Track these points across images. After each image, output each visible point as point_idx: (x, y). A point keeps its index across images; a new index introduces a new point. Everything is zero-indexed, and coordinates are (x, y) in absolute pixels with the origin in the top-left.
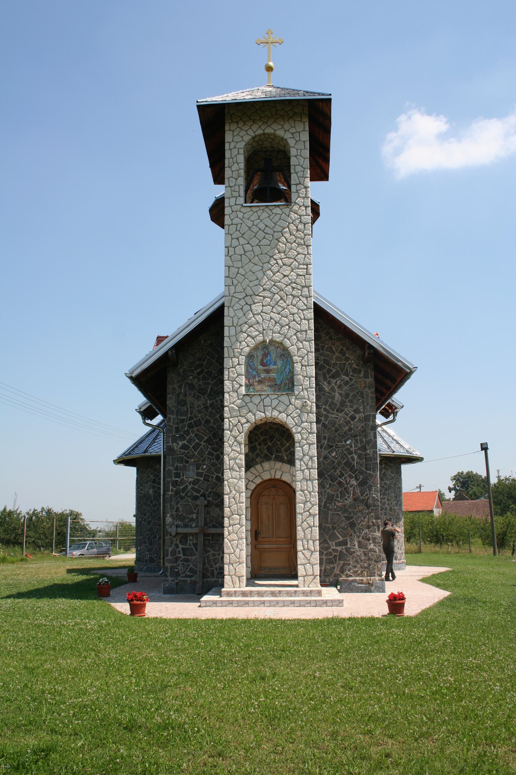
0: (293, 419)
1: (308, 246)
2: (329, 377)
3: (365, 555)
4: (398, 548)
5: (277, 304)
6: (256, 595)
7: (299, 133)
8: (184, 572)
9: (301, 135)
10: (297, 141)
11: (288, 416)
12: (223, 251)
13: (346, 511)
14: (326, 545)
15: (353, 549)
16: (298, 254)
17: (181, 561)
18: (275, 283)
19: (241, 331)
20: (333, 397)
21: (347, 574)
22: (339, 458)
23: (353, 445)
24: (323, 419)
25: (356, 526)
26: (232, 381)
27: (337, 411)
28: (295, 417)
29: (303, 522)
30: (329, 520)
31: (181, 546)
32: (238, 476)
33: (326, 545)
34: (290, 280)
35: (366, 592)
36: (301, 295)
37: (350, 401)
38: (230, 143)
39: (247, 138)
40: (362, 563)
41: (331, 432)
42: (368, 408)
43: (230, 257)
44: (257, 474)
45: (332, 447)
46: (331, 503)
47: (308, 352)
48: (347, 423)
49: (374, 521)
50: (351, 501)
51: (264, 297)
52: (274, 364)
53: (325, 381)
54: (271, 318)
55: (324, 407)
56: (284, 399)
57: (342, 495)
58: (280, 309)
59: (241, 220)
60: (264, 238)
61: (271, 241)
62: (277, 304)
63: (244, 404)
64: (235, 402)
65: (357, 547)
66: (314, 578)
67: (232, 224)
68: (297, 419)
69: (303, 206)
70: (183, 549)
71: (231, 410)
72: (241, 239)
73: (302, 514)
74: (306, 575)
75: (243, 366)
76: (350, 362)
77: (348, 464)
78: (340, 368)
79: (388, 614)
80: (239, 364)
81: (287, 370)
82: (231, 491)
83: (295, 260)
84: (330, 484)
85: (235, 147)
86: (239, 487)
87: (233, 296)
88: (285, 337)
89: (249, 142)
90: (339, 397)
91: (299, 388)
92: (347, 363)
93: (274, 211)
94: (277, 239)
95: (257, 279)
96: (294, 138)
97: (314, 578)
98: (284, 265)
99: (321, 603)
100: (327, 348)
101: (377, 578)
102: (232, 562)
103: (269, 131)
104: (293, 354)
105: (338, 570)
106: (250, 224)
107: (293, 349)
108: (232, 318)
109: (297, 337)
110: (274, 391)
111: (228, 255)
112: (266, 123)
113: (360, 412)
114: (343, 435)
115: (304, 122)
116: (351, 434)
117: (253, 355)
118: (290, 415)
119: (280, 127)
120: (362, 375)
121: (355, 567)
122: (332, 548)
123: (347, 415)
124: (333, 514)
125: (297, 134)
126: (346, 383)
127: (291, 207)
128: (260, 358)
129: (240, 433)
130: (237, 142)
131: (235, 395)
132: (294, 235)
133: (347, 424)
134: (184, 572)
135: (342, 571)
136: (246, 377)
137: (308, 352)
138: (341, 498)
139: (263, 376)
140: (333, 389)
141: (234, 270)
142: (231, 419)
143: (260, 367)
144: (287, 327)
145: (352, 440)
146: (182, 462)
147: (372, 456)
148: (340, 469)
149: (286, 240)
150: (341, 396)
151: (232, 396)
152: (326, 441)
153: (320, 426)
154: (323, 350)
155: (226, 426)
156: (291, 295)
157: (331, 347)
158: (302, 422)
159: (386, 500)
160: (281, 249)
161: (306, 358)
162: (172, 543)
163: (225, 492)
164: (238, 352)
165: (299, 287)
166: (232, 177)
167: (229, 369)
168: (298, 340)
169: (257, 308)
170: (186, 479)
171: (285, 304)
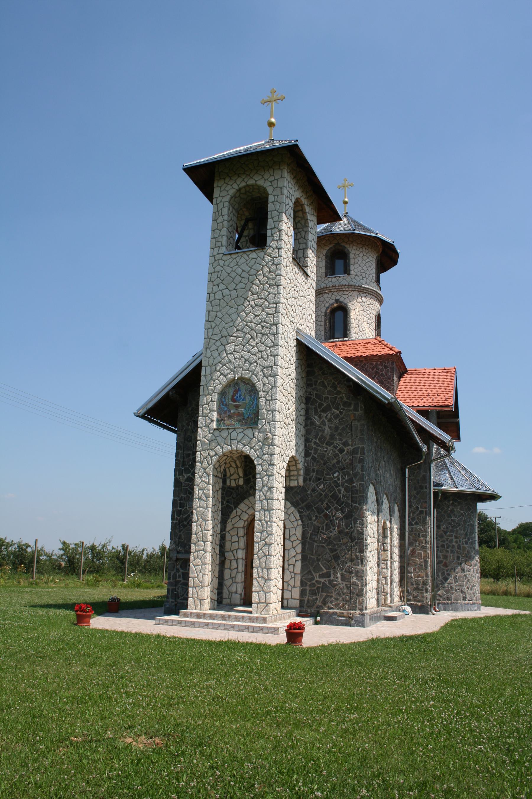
0: (255, 451)
1: (278, 286)
2: (321, 411)
3: (348, 588)
4: (468, 588)
5: (247, 343)
6: (209, 618)
7: (277, 180)
8: (183, 595)
9: (279, 182)
10: (274, 188)
11: (251, 448)
12: (205, 296)
13: (330, 543)
14: (310, 576)
15: (336, 581)
16: (270, 294)
17: (181, 584)
18: (247, 323)
19: (216, 370)
20: (323, 431)
21: (328, 606)
22: (327, 490)
23: (340, 477)
24: (312, 452)
25: (339, 559)
26: (205, 417)
27: (326, 444)
28: (258, 450)
29: (259, 551)
30: (314, 551)
31: (181, 571)
32: (205, 505)
33: (310, 576)
34: (260, 319)
35: (346, 626)
36: (269, 333)
37: (340, 434)
38: (217, 198)
39: (232, 192)
40: (344, 596)
41: (319, 465)
42: (357, 441)
43: (211, 302)
44: (250, 505)
45: (319, 479)
46: (316, 535)
47: (273, 387)
48: (336, 456)
49: (358, 554)
50: (335, 533)
51: (237, 337)
52: (243, 400)
53: (316, 415)
54: (242, 357)
55: (314, 440)
56: (249, 432)
57: (328, 527)
58: (250, 347)
59: (222, 267)
60: (241, 282)
61: (246, 284)
62: (247, 343)
63: (214, 438)
64: (206, 436)
65: (339, 579)
66: (266, 606)
67: (214, 272)
68: (259, 452)
69: (276, 248)
70: (183, 573)
71: (203, 443)
72: (221, 285)
73: (258, 543)
74: (260, 602)
75: (216, 403)
76: (341, 395)
77: (335, 497)
78: (331, 402)
79: (287, 643)
80: (212, 401)
81: (254, 405)
82: (198, 519)
83: (266, 300)
84: (316, 516)
85: (221, 202)
86: (205, 515)
87: (211, 338)
88: (253, 374)
89: (235, 195)
90: (329, 430)
91: (263, 422)
92: (338, 396)
93: (251, 256)
94: (251, 282)
95: (232, 321)
96: (272, 185)
97: (266, 606)
98: (256, 305)
99: (258, 629)
100: (320, 383)
101: (358, 612)
102: (195, 585)
103: (251, 182)
104: (259, 389)
105: (321, 601)
106: (229, 270)
107: (259, 385)
108: (209, 358)
109: (263, 373)
110: (242, 425)
111: (209, 301)
112: (249, 175)
113: (349, 445)
114: (331, 468)
115: (282, 170)
116: (339, 467)
117: (226, 392)
118: (253, 448)
119: (261, 177)
120: (352, 408)
121: (337, 599)
122: (316, 579)
123: (336, 447)
124: (318, 546)
125: (276, 181)
126: (337, 416)
127: (265, 251)
128: (231, 394)
129: (209, 465)
130: (223, 197)
131: (207, 429)
132: (267, 277)
133: (335, 457)
134: (183, 595)
135: (324, 603)
136: (218, 413)
137: (273, 387)
138: (327, 530)
139: (232, 411)
140: (323, 423)
141: (213, 314)
142: (202, 452)
143: (231, 403)
144: (255, 364)
145: (339, 473)
146: (186, 493)
147: (358, 488)
148: (326, 501)
149: (260, 282)
150: (331, 429)
151: (204, 431)
152: (315, 474)
153: (309, 459)
154: (316, 385)
155: (198, 459)
156: (261, 333)
157: (323, 382)
158: (264, 454)
159: (453, 537)
160: (254, 291)
161: (270, 393)
162: (174, 567)
163: (193, 520)
164: (212, 390)
165: (268, 325)
166: (217, 229)
167: (203, 405)
168: (265, 376)
169: (230, 348)
170: (188, 509)
171: (254, 342)
